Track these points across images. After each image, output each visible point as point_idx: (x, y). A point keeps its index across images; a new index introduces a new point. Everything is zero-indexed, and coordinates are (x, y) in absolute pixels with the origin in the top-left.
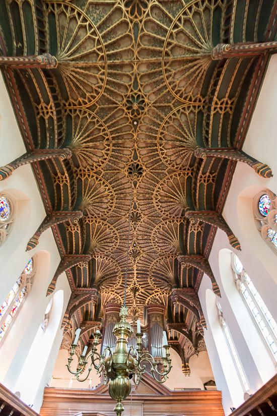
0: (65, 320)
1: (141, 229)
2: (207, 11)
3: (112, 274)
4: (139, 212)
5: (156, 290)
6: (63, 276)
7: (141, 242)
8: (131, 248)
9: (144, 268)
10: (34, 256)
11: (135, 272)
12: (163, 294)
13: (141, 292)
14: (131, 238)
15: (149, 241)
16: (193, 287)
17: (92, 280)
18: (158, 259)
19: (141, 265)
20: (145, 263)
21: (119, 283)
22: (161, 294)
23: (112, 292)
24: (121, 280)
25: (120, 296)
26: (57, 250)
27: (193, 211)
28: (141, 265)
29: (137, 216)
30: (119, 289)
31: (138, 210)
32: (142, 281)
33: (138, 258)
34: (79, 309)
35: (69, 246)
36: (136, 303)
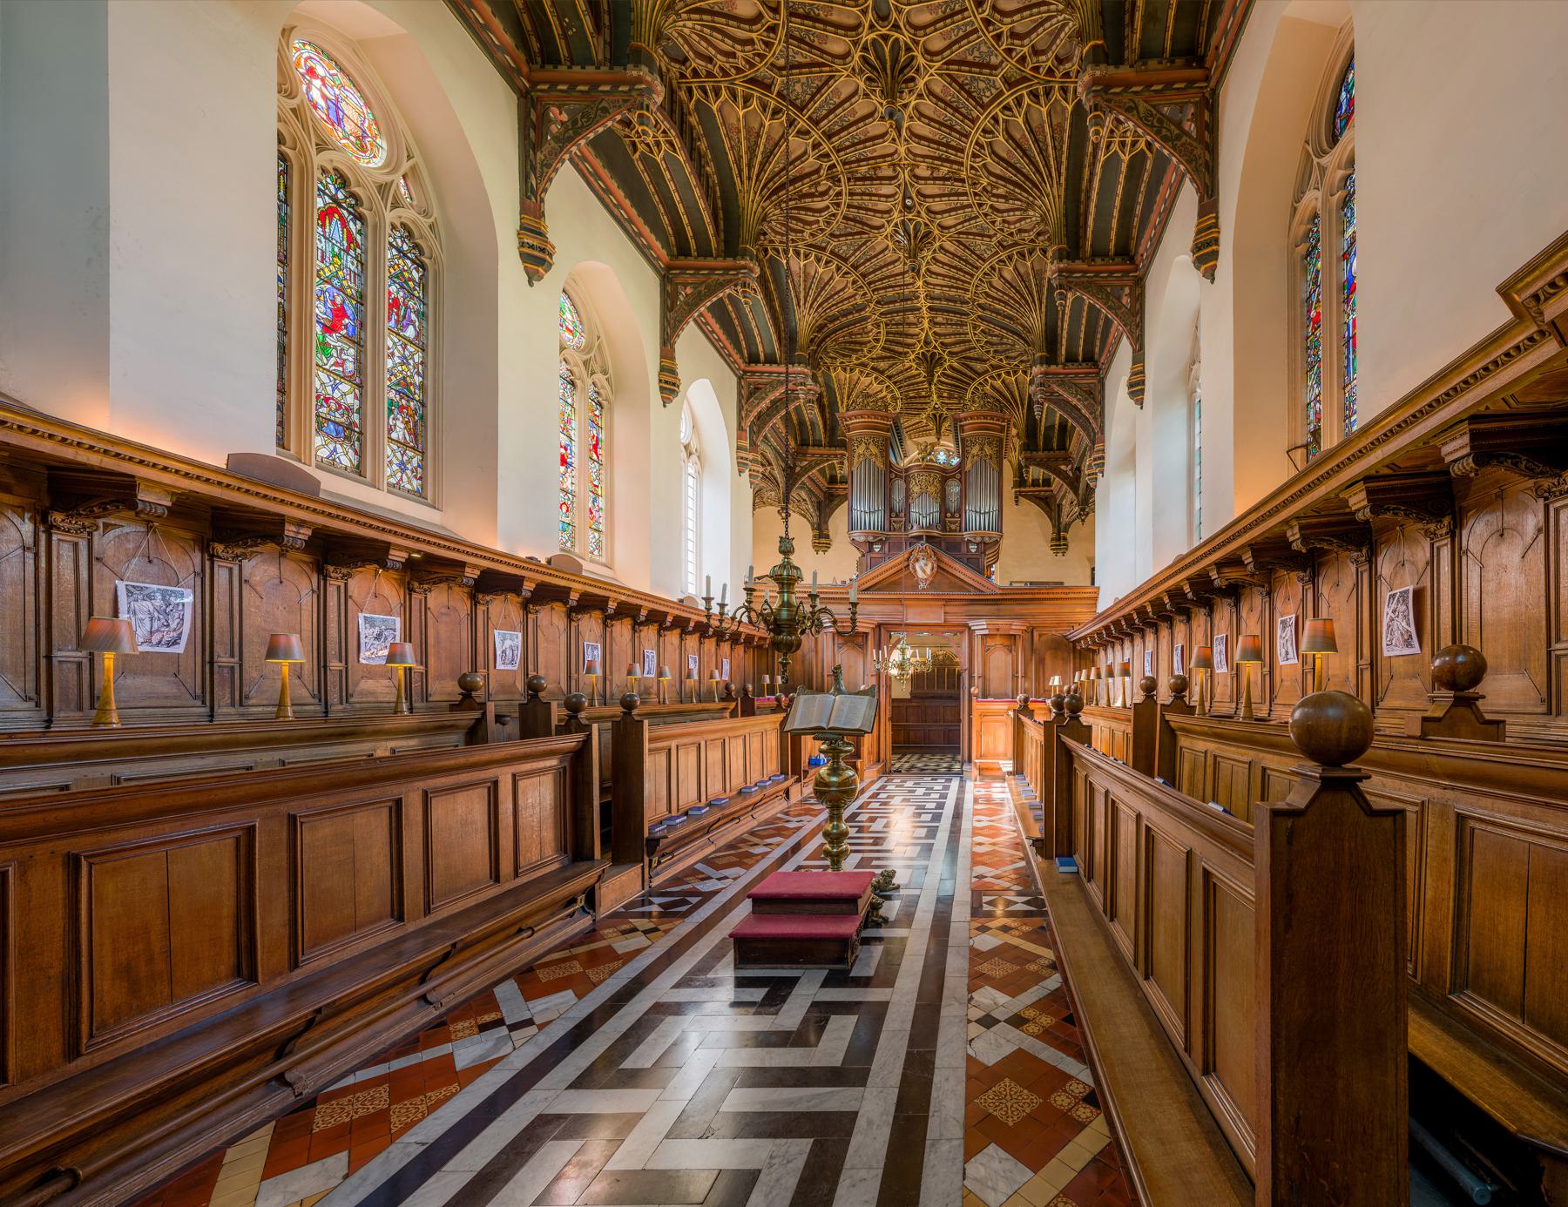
0: (743, 454)
1: (922, 128)
2: (884, 13)
3: (846, 313)
4: (905, 37)
5: (994, 362)
6: (691, 341)
7: (930, 189)
8: (896, 216)
9: (953, 293)
10: (566, 282)
11: (923, 303)
12: (1015, 372)
13: (951, 367)
14: (890, 173)
15: (958, 187)
16: (1093, 361)
17: (788, 337)
18: (994, 260)
19: (939, 281)
20: (961, 265)
21: (877, 341)
22: (1008, 373)
23: (862, 369)
24: (883, 330)
25: (895, 383)
26: (631, 246)
27: (1112, 70)
28: (939, 281)
29: (895, 60)
30: (883, 358)
31: (896, 27)
32: (950, 335)
33: (927, 254)
34: (777, 420)
35: (665, 220)
36: (940, 397)
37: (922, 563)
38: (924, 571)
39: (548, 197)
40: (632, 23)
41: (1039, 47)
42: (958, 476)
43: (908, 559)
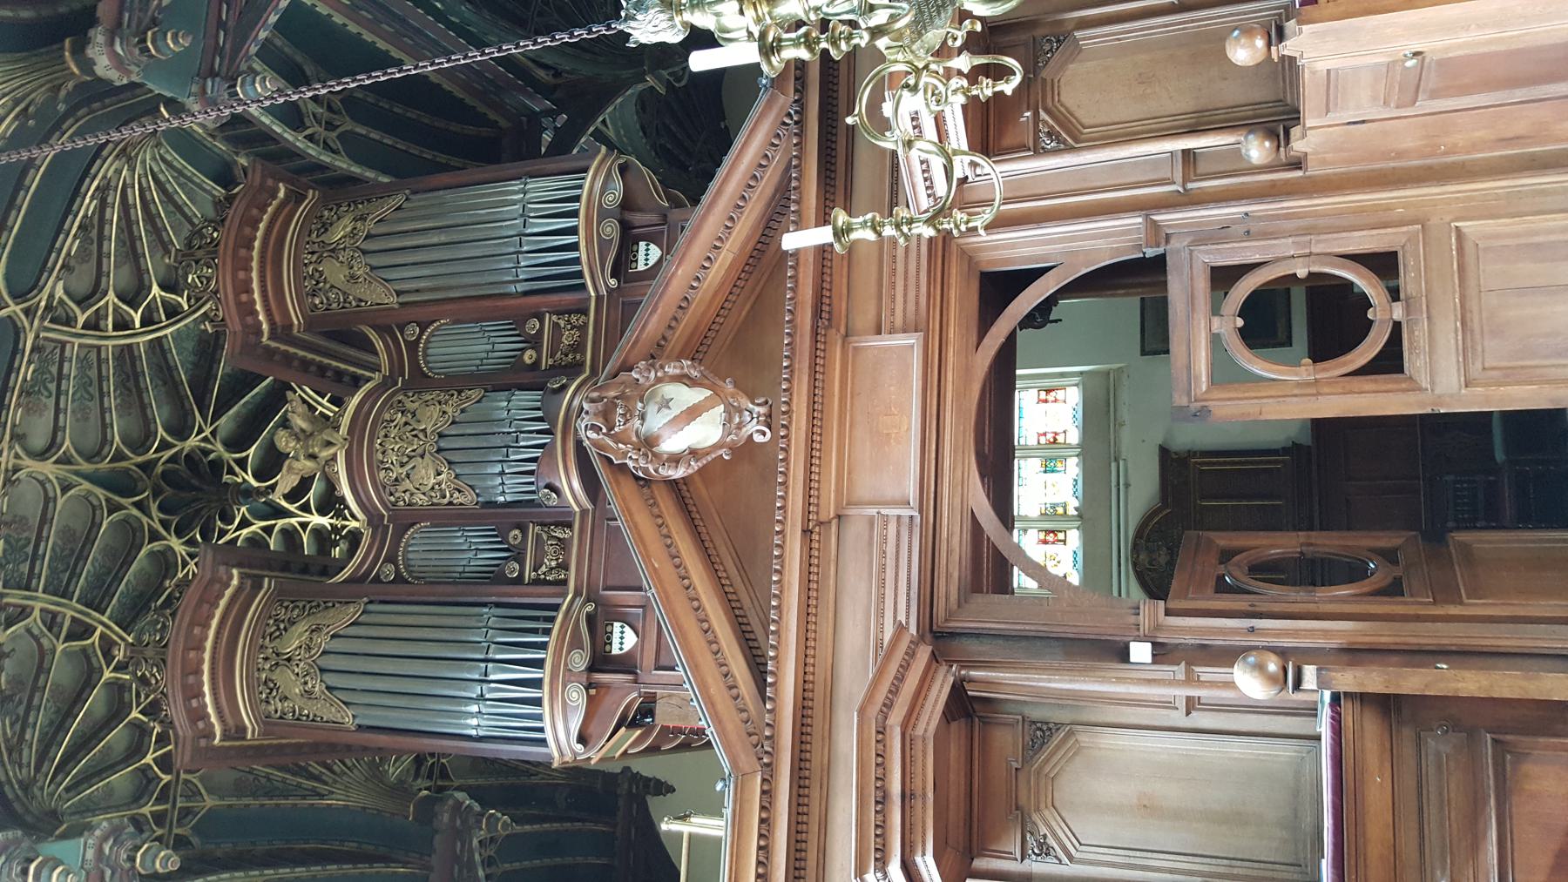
37: (656, 421)
38: (692, 413)
39: (644, 774)
40: (1435, 536)
41: (136, 433)
42: (412, 331)
43: (644, 482)
